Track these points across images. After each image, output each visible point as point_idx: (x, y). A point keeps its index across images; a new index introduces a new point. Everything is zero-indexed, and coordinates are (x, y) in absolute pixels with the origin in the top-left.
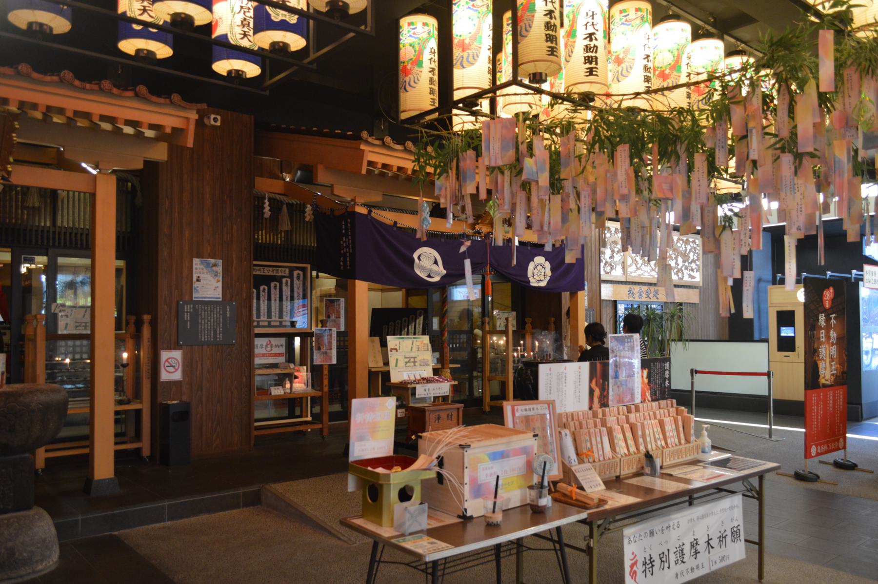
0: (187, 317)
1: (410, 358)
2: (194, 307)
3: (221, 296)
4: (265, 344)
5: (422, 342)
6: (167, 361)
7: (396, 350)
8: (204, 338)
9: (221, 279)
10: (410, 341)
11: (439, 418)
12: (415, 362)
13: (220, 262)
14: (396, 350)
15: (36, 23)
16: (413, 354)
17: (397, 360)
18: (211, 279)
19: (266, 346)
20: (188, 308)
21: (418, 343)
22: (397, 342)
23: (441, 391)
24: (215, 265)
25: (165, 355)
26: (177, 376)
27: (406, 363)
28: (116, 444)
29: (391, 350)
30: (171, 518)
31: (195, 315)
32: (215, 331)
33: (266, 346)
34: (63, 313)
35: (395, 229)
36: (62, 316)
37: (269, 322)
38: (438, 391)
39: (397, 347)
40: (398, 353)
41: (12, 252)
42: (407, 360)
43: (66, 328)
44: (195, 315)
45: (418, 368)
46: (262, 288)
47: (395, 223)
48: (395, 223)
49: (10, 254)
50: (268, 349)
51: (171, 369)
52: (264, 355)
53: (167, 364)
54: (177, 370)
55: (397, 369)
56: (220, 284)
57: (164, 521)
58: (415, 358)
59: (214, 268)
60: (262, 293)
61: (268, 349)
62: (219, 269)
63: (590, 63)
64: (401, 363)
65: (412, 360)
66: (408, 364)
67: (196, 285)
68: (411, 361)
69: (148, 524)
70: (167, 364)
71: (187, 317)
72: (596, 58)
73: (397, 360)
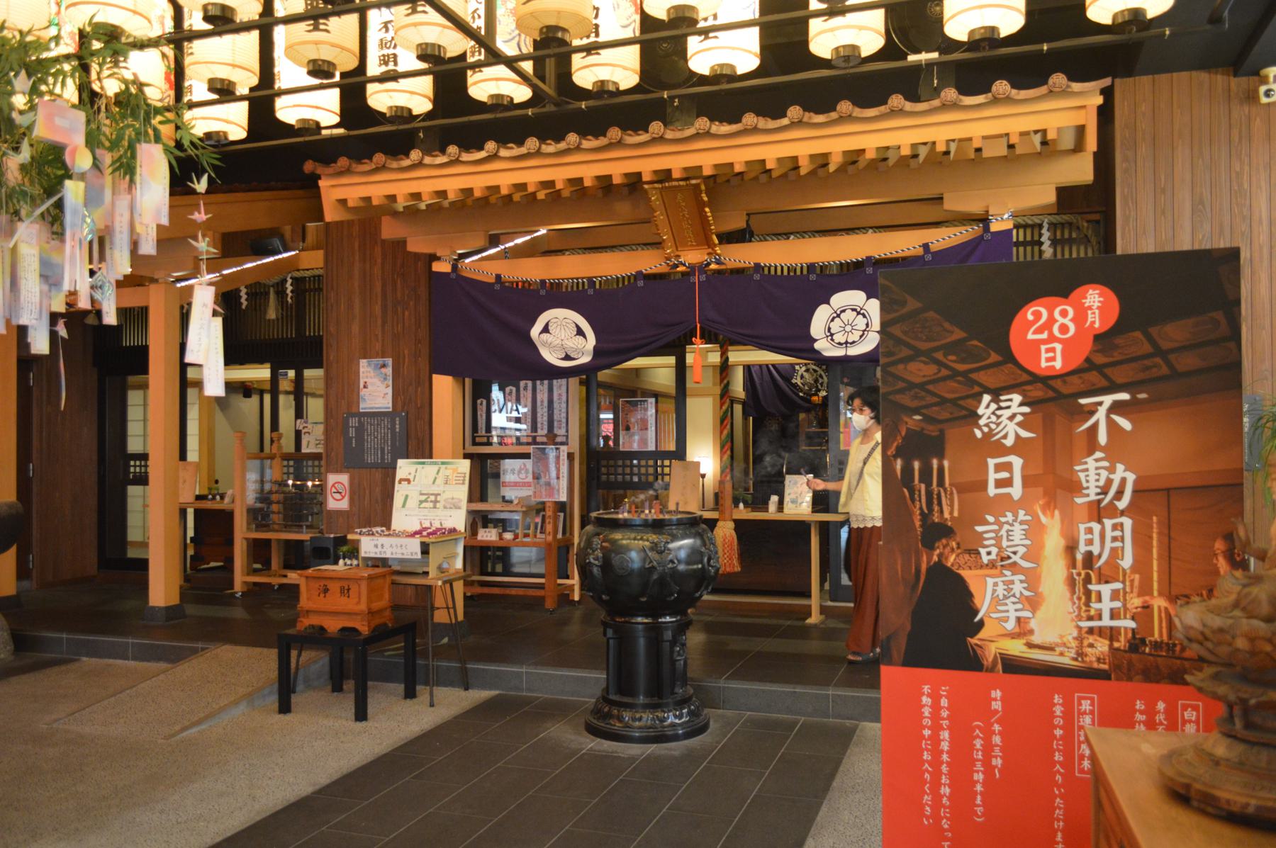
0: (352, 433)
2: (360, 421)
3: (390, 405)
4: (517, 468)
5: (455, 470)
7: (409, 481)
8: (370, 459)
9: (390, 383)
10: (435, 468)
11: (326, 590)
12: (436, 502)
13: (389, 361)
14: (409, 481)
15: (844, 47)
16: (435, 490)
17: (407, 496)
18: (379, 383)
19: (519, 472)
20: (353, 422)
21: (448, 472)
24: (384, 366)
26: (344, 505)
27: (421, 502)
30: (135, 659)
31: (360, 430)
32: (383, 450)
33: (519, 472)
35: (497, 287)
37: (534, 438)
38: (399, 550)
39: (411, 478)
42: (423, 498)
44: (360, 430)
47: (498, 277)
48: (926, 246)
50: (523, 476)
51: (338, 496)
52: (516, 484)
55: (404, 511)
56: (390, 390)
57: (126, 658)
59: (383, 370)
61: (523, 476)
62: (389, 371)
63: (386, 63)
64: (412, 503)
65: (432, 498)
66: (424, 505)
67: (363, 392)
68: (432, 500)
69: (100, 657)
71: (352, 433)
72: (395, 56)
73: (407, 496)
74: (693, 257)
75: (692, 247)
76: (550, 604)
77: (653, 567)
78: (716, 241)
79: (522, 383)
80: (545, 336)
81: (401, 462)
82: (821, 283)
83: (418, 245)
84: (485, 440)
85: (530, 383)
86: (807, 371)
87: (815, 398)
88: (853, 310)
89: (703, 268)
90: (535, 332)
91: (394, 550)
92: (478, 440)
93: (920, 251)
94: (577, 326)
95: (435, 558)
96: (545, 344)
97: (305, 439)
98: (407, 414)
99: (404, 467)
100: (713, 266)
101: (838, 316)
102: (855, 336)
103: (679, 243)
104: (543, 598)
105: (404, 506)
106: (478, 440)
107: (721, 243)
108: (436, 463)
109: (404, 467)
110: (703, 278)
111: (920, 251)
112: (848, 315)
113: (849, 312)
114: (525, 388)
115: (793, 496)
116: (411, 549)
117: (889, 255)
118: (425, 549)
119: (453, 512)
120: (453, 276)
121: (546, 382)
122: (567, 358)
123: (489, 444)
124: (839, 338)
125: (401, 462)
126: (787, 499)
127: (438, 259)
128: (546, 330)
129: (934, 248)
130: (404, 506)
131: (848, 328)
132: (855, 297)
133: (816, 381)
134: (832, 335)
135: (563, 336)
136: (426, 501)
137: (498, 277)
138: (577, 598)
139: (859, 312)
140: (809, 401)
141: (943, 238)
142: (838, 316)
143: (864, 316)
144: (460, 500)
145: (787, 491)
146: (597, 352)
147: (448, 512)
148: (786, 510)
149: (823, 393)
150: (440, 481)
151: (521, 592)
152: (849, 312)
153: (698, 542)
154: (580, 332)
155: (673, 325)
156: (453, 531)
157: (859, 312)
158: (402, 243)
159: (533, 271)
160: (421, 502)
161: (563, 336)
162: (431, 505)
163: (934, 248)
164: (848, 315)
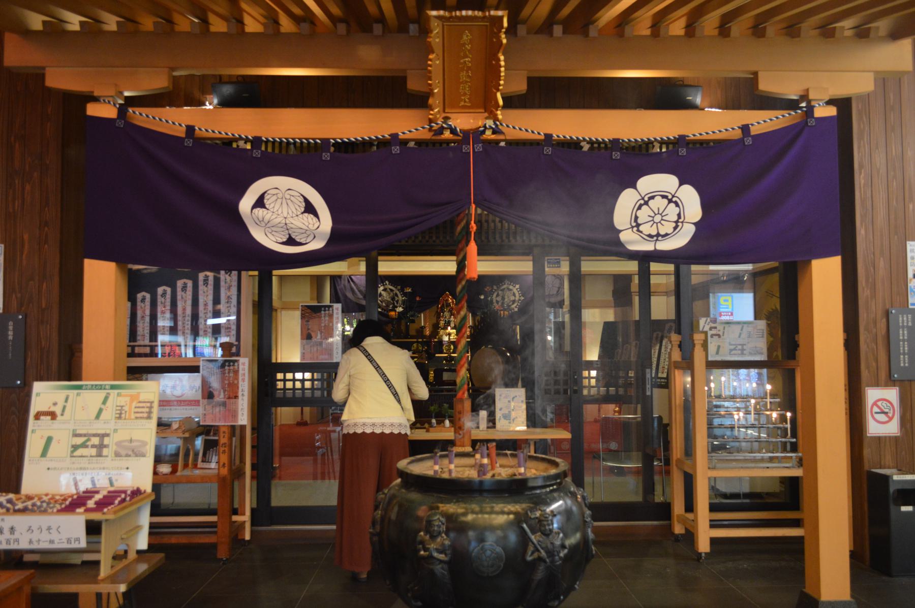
1: (89, 436)
6: (875, 404)
7: (53, 415)
10: (101, 394)
12: (101, 447)
14: (53, 415)
16: (99, 427)
17: (49, 440)
21: (122, 401)
22: (60, 396)
23: (55, 536)
25: (872, 395)
26: (892, 428)
27: (75, 447)
28: (99, 542)
29: (38, 416)
34: (714, 332)
35: (189, 143)
36: (712, 336)
39: (58, 410)
40: (56, 424)
41: (533, 261)
43: (717, 353)
45: (109, 461)
46: (160, 290)
47: (190, 129)
48: (745, 129)
49: (531, 263)
51: (882, 417)
53: (876, 409)
54: (891, 419)
55: (45, 463)
58: (103, 436)
60: (160, 299)
64: (59, 449)
66: (80, 452)
70: (876, 409)
73: (49, 440)
74: (463, 121)
75: (465, 109)
76: (223, 553)
77: (540, 559)
78: (501, 102)
79: (201, 276)
80: (259, 212)
81: (38, 387)
82: (629, 162)
83: (62, 78)
84: (148, 350)
85: (211, 275)
86: (385, 290)
87: (393, 313)
88: (664, 197)
89: (477, 133)
90: (245, 204)
91: (35, 536)
92: (137, 350)
93: (738, 134)
94: (306, 201)
95: (109, 545)
96: (258, 222)
97: (79, 484)
98: (26, 317)
99: (44, 394)
100: (488, 134)
101: (646, 203)
102: (667, 228)
103: (451, 103)
104: (214, 546)
105: (44, 454)
106: (137, 350)
107: (505, 106)
108: (101, 388)
109: (44, 394)
110: (479, 147)
111: (738, 134)
112: (658, 203)
113: (658, 198)
114: (184, 288)
115: (505, 411)
116: (68, 532)
117: (698, 137)
118: (93, 529)
119: (133, 462)
120: (120, 123)
121: (235, 273)
122: (291, 242)
123: (153, 354)
124: (646, 229)
125: (38, 387)
126: (498, 414)
127: (95, 99)
128: (260, 203)
129: (754, 131)
130: (44, 454)
131: (658, 218)
132: (667, 182)
133: (393, 299)
134: (638, 225)
135: (284, 212)
136: (84, 445)
137: (190, 129)
138: (247, 537)
139: (671, 200)
140: (387, 316)
141: (763, 121)
142: (646, 203)
143: (677, 205)
144: (144, 444)
145: (499, 404)
146: (335, 236)
147: (124, 462)
148: (499, 425)
149: (400, 309)
150: (109, 413)
151: (183, 540)
152: (658, 198)
153: (569, 502)
154: (310, 209)
155: (447, 203)
156: (137, 492)
157: (671, 200)
158: (39, 76)
159: (245, 124)
160: (75, 447)
161: (284, 212)
162: (94, 451)
163: (754, 131)
164: (658, 203)
